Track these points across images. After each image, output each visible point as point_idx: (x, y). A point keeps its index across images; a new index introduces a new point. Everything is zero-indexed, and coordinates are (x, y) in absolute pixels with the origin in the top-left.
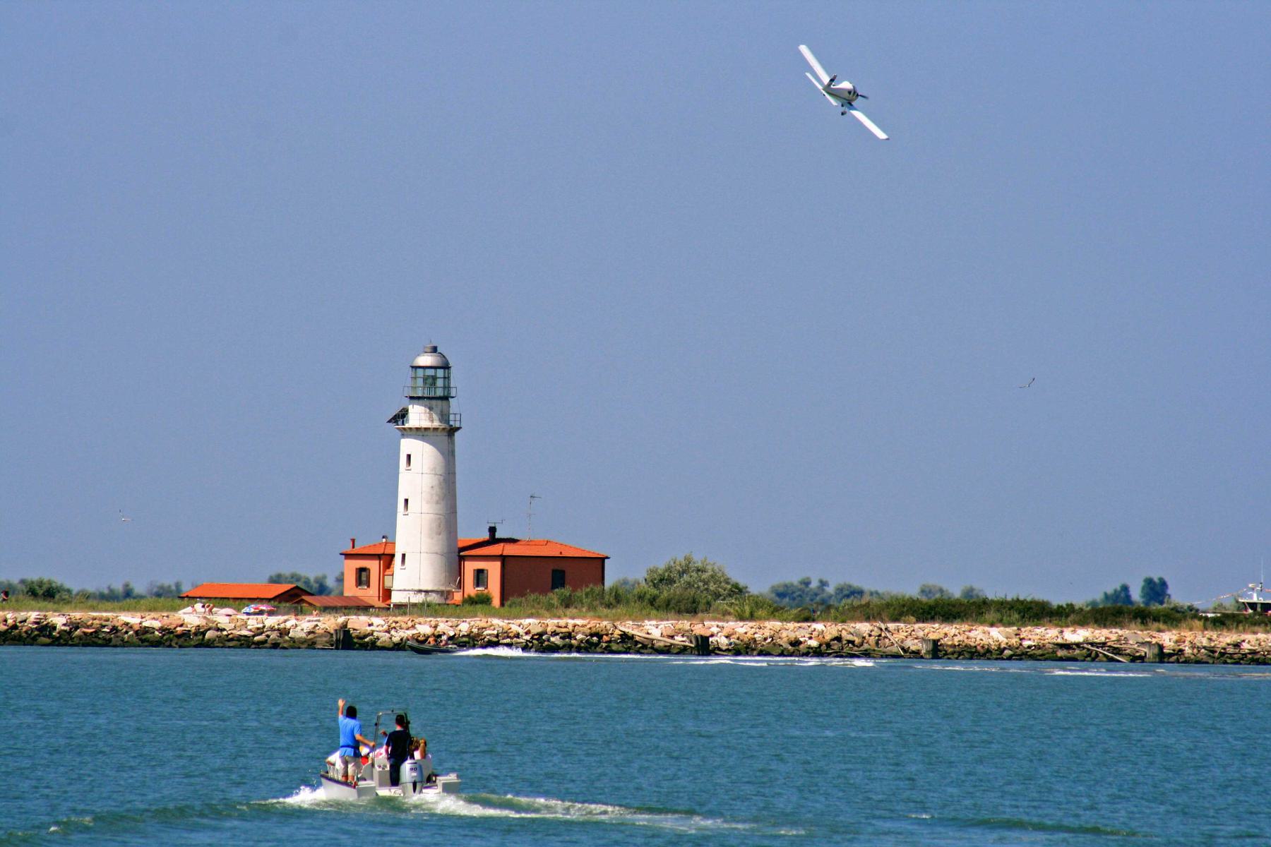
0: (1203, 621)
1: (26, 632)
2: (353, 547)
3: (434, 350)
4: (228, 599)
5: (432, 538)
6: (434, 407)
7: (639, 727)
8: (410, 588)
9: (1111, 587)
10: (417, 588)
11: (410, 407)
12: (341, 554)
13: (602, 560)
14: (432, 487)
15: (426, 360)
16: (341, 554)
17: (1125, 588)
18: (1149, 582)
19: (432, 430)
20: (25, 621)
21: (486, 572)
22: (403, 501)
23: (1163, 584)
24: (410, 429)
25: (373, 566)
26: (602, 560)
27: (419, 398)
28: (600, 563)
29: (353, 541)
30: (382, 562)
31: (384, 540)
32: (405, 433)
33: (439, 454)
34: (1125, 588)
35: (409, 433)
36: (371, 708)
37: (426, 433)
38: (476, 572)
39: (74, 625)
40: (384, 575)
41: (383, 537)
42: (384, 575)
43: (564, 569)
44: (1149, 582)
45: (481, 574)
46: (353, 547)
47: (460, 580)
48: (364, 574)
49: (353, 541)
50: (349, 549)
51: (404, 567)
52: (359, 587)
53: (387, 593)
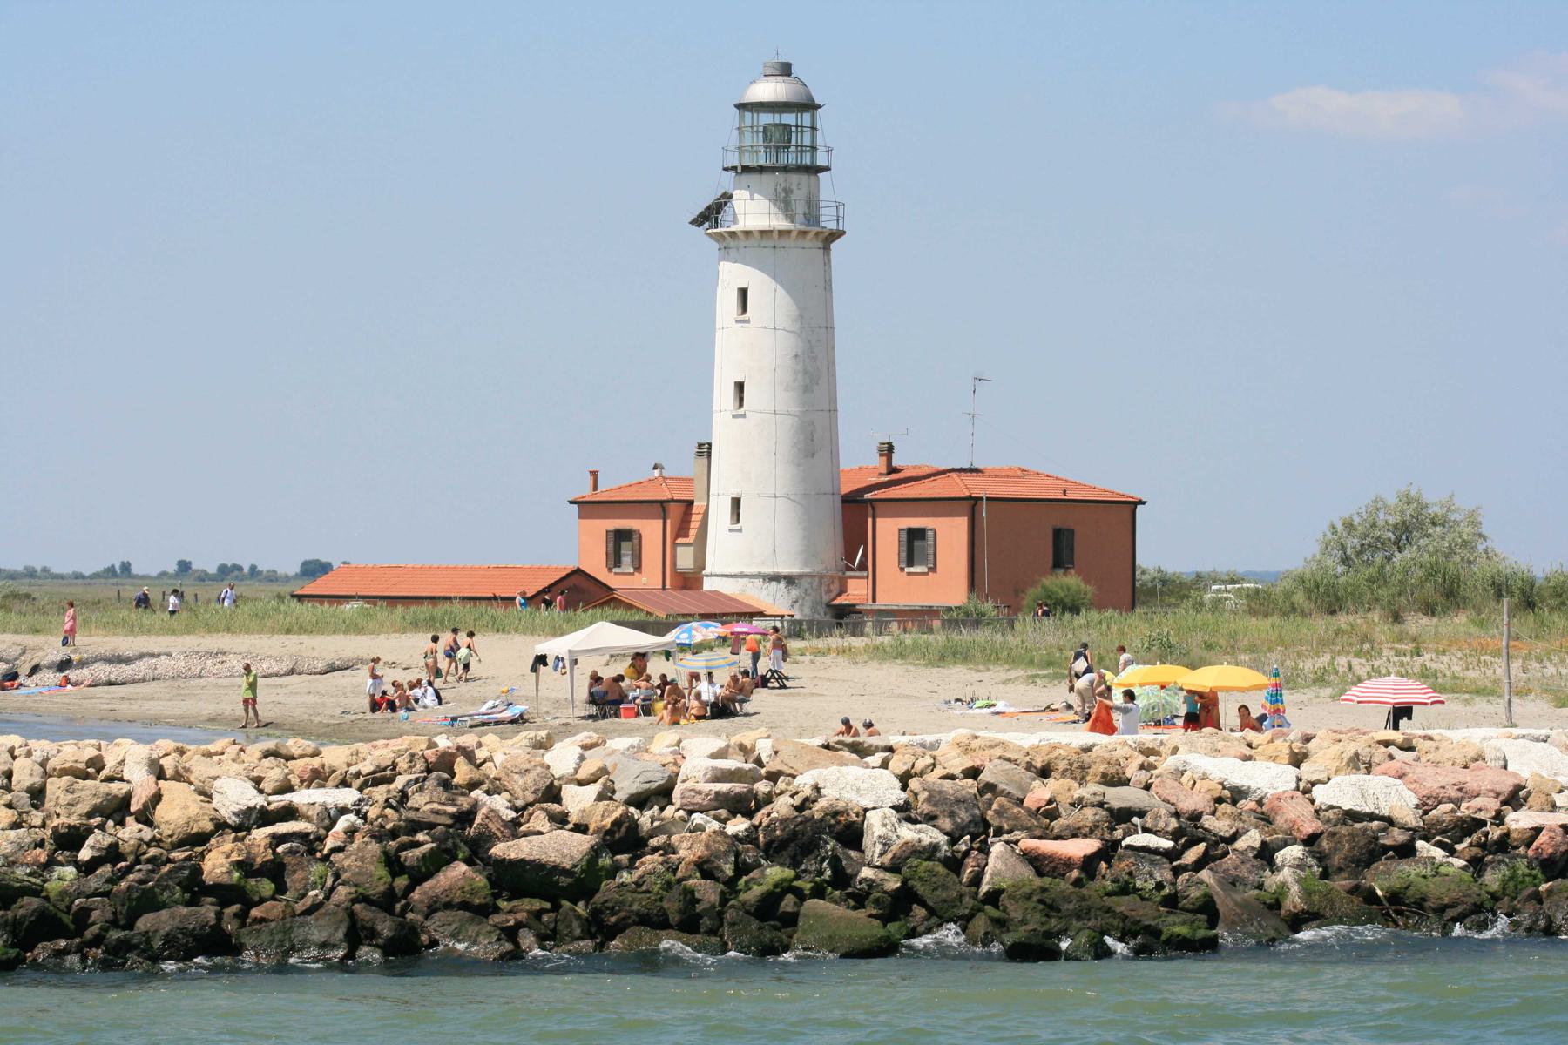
0: (783, 582)
1: (705, 868)
2: (595, 488)
3: (785, 70)
4: (449, 598)
5: (799, 465)
6: (794, 187)
7: (1359, 841)
8: (754, 570)
9: (107, 565)
10: (769, 570)
11: (738, 195)
12: (571, 502)
13: (1136, 503)
14: (796, 356)
15: (769, 90)
16: (571, 502)
17: (113, 566)
18: (123, 563)
19: (794, 235)
20: (663, 794)
21: (930, 533)
22: (731, 391)
23: (129, 564)
24: (747, 233)
25: (650, 530)
26: (1136, 503)
27: (761, 169)
28: (1126, 511)
29: (594, 474)
30: (669, 521)
31: (656, 473)
32: (732, 243)
33: (781, 291)
34: (113, 566)
35: (743, 242)
36: (1038, 882)
37: (779, 243)
38: (904, 534)
39: (963, 816)
40: (675, 545)
41: (655, 468)
42: (675, 545)
43: (1072, 528)
44: (123, 563)
45: (917, 544)
46: (595, 488)
47: (865, 554)
48: (626, 548)
49: (594, 474)
50: (585, 492)
51: (737, 526)
52: (615, 570)
53: (689, 581)
